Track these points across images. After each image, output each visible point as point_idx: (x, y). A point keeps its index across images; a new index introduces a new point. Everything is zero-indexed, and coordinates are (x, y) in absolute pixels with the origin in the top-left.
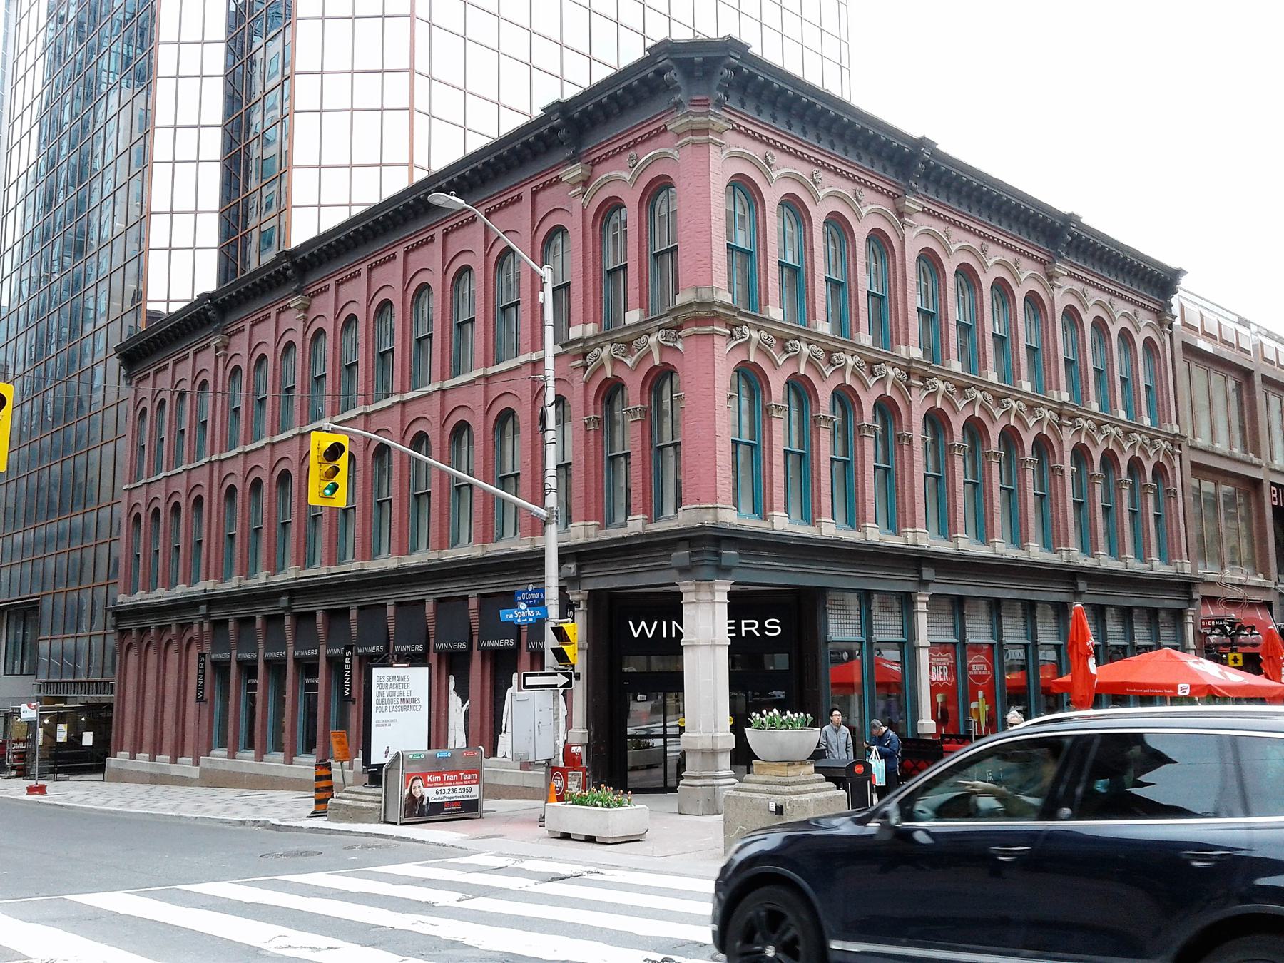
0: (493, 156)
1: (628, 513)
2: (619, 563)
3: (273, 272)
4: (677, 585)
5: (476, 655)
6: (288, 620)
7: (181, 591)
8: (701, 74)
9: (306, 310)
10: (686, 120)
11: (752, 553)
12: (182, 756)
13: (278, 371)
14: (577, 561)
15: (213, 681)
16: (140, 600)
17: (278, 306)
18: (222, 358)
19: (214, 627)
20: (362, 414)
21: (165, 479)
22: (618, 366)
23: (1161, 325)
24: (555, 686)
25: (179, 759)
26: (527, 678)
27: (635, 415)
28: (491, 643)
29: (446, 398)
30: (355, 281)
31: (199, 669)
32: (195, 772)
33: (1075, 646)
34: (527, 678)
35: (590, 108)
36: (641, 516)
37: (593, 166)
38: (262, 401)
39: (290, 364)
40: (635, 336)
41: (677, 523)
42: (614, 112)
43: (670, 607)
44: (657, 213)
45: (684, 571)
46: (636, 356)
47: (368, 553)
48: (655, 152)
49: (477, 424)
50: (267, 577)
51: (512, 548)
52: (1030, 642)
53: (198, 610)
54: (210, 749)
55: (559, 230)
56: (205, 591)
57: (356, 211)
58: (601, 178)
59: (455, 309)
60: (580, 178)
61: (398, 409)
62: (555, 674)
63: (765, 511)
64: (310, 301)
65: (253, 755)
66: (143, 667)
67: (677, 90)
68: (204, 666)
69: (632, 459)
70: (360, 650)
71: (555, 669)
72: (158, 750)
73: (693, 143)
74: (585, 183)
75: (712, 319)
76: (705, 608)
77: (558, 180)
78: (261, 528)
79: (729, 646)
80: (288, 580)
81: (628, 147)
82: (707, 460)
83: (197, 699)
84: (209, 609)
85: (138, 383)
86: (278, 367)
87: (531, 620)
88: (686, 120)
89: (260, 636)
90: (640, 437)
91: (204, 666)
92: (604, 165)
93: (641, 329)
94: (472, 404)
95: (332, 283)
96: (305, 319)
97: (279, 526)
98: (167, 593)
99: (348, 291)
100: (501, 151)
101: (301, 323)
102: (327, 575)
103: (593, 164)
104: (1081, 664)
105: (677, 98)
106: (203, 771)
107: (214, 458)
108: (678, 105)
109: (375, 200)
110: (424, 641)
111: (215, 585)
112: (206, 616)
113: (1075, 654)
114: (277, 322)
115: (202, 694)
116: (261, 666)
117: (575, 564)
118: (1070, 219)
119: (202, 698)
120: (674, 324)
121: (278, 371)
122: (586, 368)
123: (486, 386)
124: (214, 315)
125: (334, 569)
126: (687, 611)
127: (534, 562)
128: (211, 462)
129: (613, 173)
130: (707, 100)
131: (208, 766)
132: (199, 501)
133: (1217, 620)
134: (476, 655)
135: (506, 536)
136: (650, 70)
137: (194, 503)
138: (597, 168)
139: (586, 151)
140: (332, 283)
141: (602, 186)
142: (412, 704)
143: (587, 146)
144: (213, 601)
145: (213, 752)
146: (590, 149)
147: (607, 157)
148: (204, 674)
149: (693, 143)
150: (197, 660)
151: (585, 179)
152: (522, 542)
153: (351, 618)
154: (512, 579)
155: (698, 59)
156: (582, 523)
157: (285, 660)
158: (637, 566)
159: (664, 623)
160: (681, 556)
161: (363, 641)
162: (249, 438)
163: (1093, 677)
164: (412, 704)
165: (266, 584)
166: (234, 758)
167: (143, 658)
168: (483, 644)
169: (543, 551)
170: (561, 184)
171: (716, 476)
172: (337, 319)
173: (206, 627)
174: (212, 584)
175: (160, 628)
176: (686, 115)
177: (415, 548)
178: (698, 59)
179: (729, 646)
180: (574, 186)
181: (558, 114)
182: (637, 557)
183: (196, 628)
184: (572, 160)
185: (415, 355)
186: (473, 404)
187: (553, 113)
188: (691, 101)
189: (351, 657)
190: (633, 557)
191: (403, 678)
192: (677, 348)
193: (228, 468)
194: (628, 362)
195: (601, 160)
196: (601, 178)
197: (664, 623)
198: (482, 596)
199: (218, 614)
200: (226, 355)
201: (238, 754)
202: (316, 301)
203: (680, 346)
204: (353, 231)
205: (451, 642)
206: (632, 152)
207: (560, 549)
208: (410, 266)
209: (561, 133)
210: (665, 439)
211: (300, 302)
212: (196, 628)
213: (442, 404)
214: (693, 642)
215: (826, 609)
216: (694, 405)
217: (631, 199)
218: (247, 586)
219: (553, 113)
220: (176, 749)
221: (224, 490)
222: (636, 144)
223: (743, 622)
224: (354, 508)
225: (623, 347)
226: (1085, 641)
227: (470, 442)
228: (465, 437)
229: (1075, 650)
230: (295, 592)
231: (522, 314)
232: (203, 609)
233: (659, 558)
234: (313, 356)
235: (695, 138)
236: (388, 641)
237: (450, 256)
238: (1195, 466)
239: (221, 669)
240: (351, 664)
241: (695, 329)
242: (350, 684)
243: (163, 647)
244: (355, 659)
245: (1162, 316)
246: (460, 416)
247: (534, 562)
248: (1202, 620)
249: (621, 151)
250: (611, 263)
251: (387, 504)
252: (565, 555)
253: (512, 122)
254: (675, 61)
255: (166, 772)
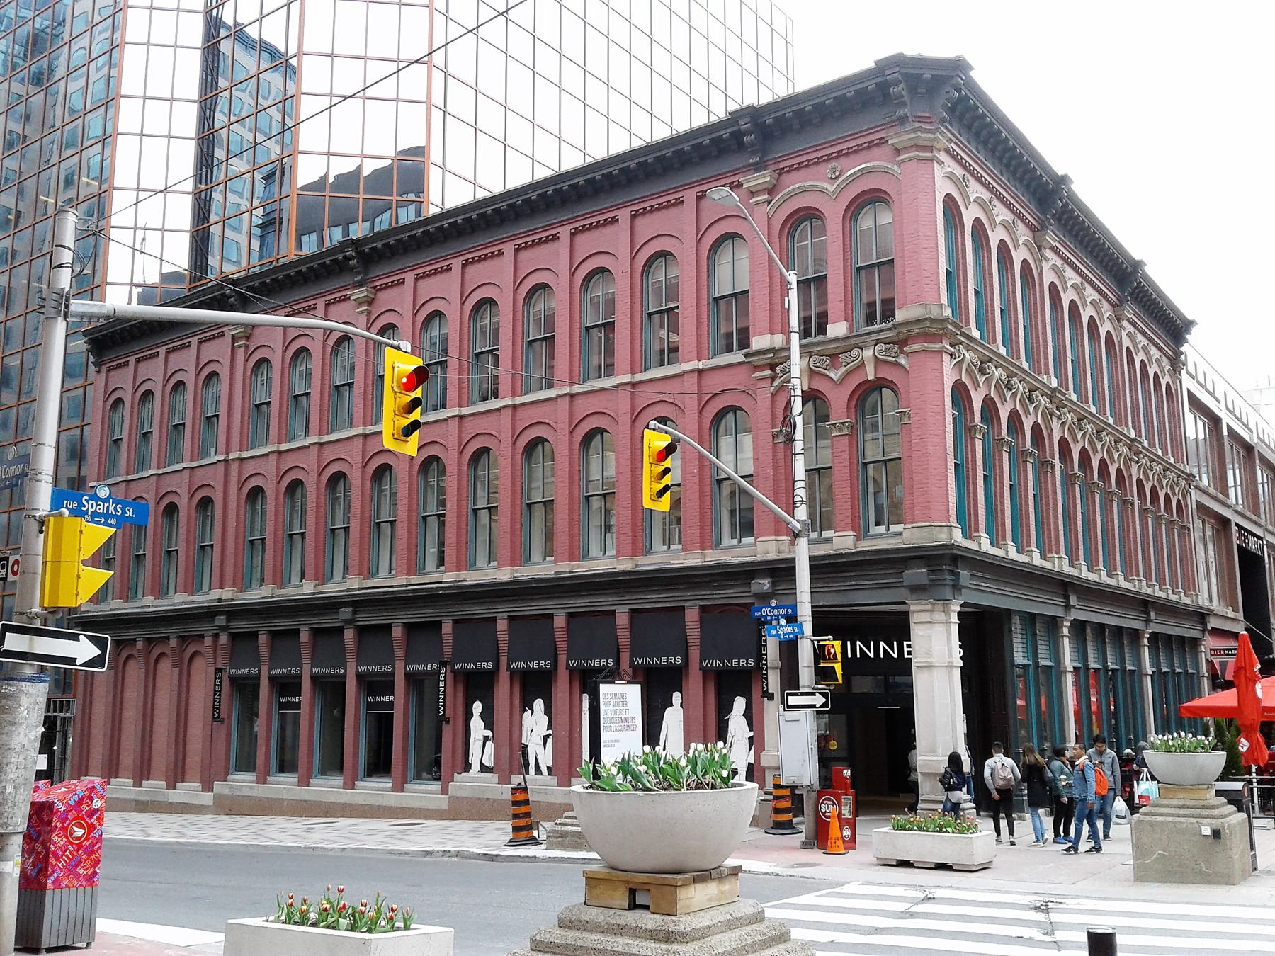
0: (652, 156)
1: (303, 577)
2: (827, 580)
3: (328, 261)
4: (906, 603)
5: (504, 676)
6: (349, 634)
7: (180, 600)
8: (924, 91)
9: (370, 302)
10: (914, 135)
11: (981, 574)
12: (183, 781)
13: (327, 367)
14: (771, 577)
15: (231, 700)
16: (272, 597)
17: (576, 225)
18: (243, 349)
19: (233, 639)
20: (456, 416)
21: (155, 478)
22: (816, 380)
23: (1175, 371)
24: (814, 706)
25: (179, 785)
26: (789, 697)
27: (840, 429)
28: (240, 672)
29: (574, 403)
30: (185, 351)
31: (215, 685)
32: (207, 799)
33: (1243, 672)
34: (789, 697)
35: (670, 154)
36: (852, 533)
37: (780, 174)
38: (117, 442)
39: (118, 415)
40: (842, 350)
41: (900, 541)
42: (713, 154)
43: (898, 627)
44: (650, 279)
45: (918, 590)
46: (843, 369)
47: (463, 564)
48: (868, 165)
49: (310, 480)
50: (315, 587)
51: (672, 562)
52: (1101, 667)
53: (214, 620)
54: (227, 773)
55: (214, 374)
56: (220, 600)
57: (481, 194)
58: (793, 187)
59: (204, 405)
60: (766, 186)
61: (186, 473)
62: (813, 694)
63: (970, 531)
64: (375, 294)
65: (297, 780)
66: (120, 683)
67: (904, 104)
68: (220, 682)
69: (307, 540)
70: (458, 666)
71: (813, 689)
72: (84, 768)
73: (919, 159)
74: (771, 191)
75: (941, 335)
76: (940, 628)
77: (347, 298)
78: (395, 520)
79: (961, 667)
80: (348, 590)
81: (830, 158)
82: (937, 478)
83: (214, 718)
84: (228, 621)
85: (109, 370)
86: (328, 362)
87: (791, 636)
88: (914, 135)
89: (306, 650)
90: (848, 452)
91: (220, 682)
92: (794, 175)
93: (850, 343)
94: (349, 456)
95: (132, 360)
96: (369, 313)
97: (328, 532)
98: (157, 602)
99: (177, 360)
100: (721, 133)
101: (363, 318)
102: (407, 586)
103: (781, 172)
104: (1250, 689)
105: (901, 113)
106: (218, 798)
107: (231, 456)
108: (902, 120)
109: (498, 189)
110: (754, 654)
111: (233, 595)
112: (222, 628)
113: (1243, 680)
114: (136, 371)
115: (218, 713)
116: (306, 684)
117: (769, 580)
118: (1137, 265)
119: (218, 717)
120: (896, 339)
121: (327, 367)
122: (773, 379)
123: (514, 415)
124: (236, 303)
125: (414, 579)
126: (917, 632)
127: (783, 571)
128: (226, 461)
129: (811, 183)
130: (930, 117)
131: (226, 791)
132: (206, 503)
133: (1227, 649)
134: (563, 675)
135: (292, 583)
136: (706, 138)
137: (197, 505)
138: (785, 178)
139: (775, 158)
140: (132, 360)
141: (791, 196)
142: (630, 724)
143: (779, 152)
144: (233, 612)
145: (229, 777)
146: (779, 157)
147: (800, 167)
148: (220, 691)
149: (919, 159)
150: (213, 676)
151: (770, 187)
152: (688, 556)
153: (443, 631)
154: (677, 594)
155: (687, 148)
156: (774, 538)
157: (258, 677)
158: (853, 583)
159: (849, 643)
160: (917, 574)
161: (457, 657)
162: (163, 460)
163: (1259, 700)
164: (630, 724)
165: (314, 594)
166: (265, 783)
167: (120, 674)
168: (573, 663)
169: (793, 560)
170: (349, 301)
171: (948, 494)
172: (198, 374)
173: (223, 639)
174: (231, 592)
175: (149, 641)
176: (914, 131)
177: (528, 560)
178: (687, 148)
179: (961, 667)
180: (360, 304)
181: (748, 119)
182: (853, 574)
183: (208, 641)
184: (758, 167)
185: (527, 357)
186: (499, 432)
187: (742, 117)
188: (915, 117)
189: (445, 673)
190: (848, 574)
191: (622, 695)
192: (901, 365)
193: (251, 468)
194: (832, 375)
195: (791, 169)
196: (793, 187)
197: (849, 643)
198: (632, 611)
199: (241, 626)
200: (247, 347)
201: (269, 779)
202: (382, 296)
203: (903, 361)
204: (450, 223)
205: (245, 668)
206: (834, 164)
207: (811, 558)
208: (704, 214)
209: (352, 262)
210: (294, 528)
211: (365, 294)
212: (208, 641)
213: (460, 431)
214: (931, 663)
215: (1011, 631)
216: (923, 421)
217: (833, 213)
218: (283, 596)
219: (742, 117)
220: (110, 769)
221: (245, 491)
222: (840, 154)
223: (905, 643)
224: (177, 550)
225: (827, 360)
226: (1252, 666)
227: (304, 496)
228: (210, 508)
229: (1243, 676)
230: (359, 603)
231: (312, 403)
232: (221, 620)
233: (864, 578)
234: (172, 407)
235: (921, 154)
236: (498, 656)
237: (139, 381)
238: (1200, 506)
239: (246, 689)
240: (445, 681)
241: (926, 345)
242: (444, 702)
243: (121, 666)
244: (450, 676)
245: (1176, 362)
246: (254, 482)
247: (783, 571)
248: (1211, 650)
249: (820, 161)
250: (258, 399)
251: (174, 553)
252: (819, 568)
253: (573, 161)
254: (905, 75)
255: (159, 798)
